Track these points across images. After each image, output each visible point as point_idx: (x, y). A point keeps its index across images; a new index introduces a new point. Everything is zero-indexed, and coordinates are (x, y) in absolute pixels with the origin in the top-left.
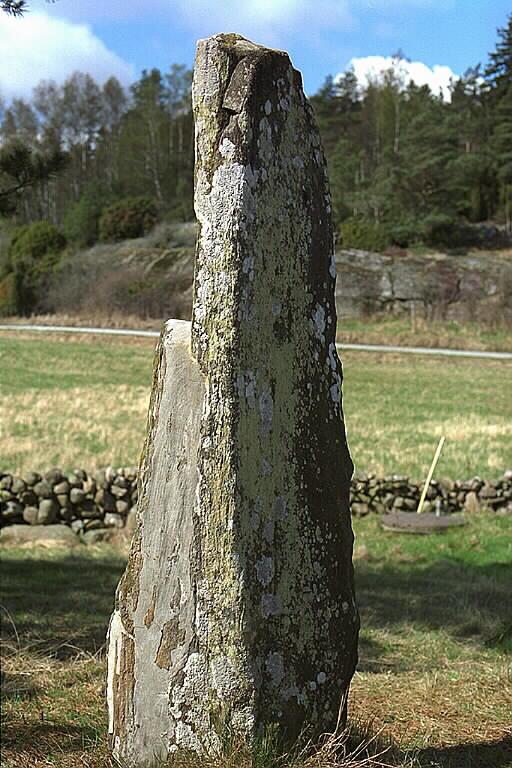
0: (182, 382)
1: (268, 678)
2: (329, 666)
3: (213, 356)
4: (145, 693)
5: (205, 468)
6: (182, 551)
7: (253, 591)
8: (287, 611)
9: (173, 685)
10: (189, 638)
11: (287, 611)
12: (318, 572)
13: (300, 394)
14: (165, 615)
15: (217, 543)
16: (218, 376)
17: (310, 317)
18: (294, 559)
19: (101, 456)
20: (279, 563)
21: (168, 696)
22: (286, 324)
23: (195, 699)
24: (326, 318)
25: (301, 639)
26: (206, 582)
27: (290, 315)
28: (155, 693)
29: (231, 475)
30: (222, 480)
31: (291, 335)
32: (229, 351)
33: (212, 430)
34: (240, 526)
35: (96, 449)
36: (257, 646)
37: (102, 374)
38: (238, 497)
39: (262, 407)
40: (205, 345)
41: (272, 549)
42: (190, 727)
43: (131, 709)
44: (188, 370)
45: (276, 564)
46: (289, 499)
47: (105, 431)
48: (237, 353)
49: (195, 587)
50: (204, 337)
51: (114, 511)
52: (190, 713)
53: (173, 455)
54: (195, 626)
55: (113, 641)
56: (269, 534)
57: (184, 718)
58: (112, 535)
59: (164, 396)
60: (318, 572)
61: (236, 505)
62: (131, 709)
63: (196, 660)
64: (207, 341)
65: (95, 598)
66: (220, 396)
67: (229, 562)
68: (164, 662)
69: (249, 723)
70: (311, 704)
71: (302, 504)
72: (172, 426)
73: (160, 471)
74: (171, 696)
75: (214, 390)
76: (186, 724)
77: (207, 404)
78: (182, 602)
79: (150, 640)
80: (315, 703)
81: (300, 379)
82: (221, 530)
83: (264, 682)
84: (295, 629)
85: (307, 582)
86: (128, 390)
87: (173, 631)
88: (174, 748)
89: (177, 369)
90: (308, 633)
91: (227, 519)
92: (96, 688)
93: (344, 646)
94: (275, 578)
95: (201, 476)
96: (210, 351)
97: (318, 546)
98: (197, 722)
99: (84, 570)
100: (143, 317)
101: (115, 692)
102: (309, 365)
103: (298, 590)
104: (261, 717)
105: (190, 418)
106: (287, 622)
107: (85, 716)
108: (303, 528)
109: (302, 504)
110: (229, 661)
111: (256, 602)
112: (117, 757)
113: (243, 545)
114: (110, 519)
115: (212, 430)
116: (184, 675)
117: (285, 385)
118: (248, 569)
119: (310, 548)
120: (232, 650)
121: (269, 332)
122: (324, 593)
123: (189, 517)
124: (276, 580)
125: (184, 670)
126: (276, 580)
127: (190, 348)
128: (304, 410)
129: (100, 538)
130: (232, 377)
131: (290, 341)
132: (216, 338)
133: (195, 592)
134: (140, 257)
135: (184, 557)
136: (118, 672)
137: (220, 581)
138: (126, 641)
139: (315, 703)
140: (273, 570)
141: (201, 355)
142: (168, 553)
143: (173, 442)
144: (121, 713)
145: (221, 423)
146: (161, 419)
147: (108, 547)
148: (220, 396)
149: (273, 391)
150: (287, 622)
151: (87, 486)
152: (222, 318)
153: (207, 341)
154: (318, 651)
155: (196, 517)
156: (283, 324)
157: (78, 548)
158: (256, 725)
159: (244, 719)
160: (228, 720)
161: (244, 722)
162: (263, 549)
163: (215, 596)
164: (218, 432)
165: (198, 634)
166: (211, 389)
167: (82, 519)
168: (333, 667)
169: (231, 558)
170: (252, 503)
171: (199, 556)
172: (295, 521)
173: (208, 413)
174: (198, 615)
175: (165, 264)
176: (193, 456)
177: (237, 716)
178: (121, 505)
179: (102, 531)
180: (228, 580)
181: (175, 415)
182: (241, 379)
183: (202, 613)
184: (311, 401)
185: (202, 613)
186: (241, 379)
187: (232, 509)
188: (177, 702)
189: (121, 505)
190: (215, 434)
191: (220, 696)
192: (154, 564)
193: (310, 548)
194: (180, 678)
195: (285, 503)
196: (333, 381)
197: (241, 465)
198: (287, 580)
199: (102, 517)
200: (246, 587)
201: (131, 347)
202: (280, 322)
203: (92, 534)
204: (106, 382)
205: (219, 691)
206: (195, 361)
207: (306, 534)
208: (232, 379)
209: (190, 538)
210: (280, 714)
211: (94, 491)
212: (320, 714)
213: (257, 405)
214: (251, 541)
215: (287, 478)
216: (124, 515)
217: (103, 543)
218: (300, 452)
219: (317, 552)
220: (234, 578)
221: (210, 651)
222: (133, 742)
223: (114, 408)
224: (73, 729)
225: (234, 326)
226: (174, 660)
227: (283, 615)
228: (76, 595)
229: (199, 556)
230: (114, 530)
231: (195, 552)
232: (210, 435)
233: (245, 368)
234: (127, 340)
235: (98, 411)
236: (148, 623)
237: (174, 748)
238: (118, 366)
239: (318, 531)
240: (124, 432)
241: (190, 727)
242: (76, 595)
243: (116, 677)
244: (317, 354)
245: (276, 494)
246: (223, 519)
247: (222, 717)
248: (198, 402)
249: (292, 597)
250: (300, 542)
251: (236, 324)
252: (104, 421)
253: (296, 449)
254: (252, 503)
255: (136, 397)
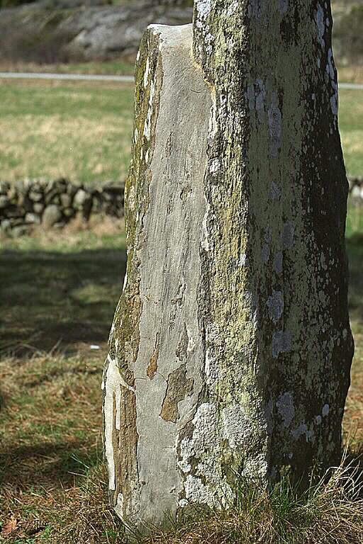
0: (183, 94)
1: (280, 421)
2: (332, 398)
3: (219, 59)
4: (151, 448)
5: (213, 195)
6: (188, 292)
7: (266, 330)
8: (296, 347)
9: (181, 438)
10: (198, 388)
11: (296, 347)
12: (323, 301)
13: (305, 106)
14: (170, 364)
15: (227, 280)
16: (226, 85)
17: (312, 18)
18: (302, 291)
19: (17, 169)
20: (288, 296)
21: (175, 449)
22: (293, 24)
23: (206, 451)
24: (325, 20)
25: (309, 374)
26: (216, 325)
27: (297, 14)
28: (161, 445)
29: (242, 203)
30: (232, 207)
31: (298, 37)
32: (238, 54)
33: (220, 150)
34: (253, 260)
35: (13, 164)
36: (269, 389)
37: (13, 107)
38: (251, 227)
39: (271, 121)
40: (210, 48)
41: (281, 282)
42: (199, 480)
43: (135, 466)
44: (191, 79)
45: (285, 297)
46: (296, 226)
47: (18, 151)
48: (248, 58)
49: (204, 331)
50: (209, 38)
51: (32, 211)
52: (200, 467)
53: (174, 182)
54: (204, 374)
55: (109, 393)
56: (278, 267)
57: (193, 472)
58: (32, 230)
59: (162, 111)
60: (323, 301)
61: (248, 237)
62: (135, 466)
63: (205, 411)
64: (212, 43)
65: (33, 289)
66: (229, 109)
67: (242, 302)
68: (170, 412)
69: (262, 470)
70: (317, 439)
71: (309, 229)
72: (172, 147)
73: (160, 199)
74: (179, 450)
75: (222, 102)
76: (197, 477)
77: (214, 118)
78: (189, 349)
79: (153, 391)
80: (321, 437)
81: (306, 87)
82: (232, 265)
83: (276, 425)
84: (303, 365)
85: (314, 313)
86: (33, 119)
87: (180, 382)
88: (183, 503)
89: (177, 78)
90: (315, 366)
91: (239, 253)
92: (58, 390)
93: (344, 374)
94: (284, 313)
95: (209, 205)
96: (217, 54)
97: (322, 273)
98: (208, 474)
99: (19, 263)
100: (40, 63)
101: (116, 448)
102: (314, 74)
103: (306, 323)
104: (272, 461)
105: (194, 137)
106: (296, 358)
107: (61, 426)
108: (310, 256)
109: (309, 229)
110: (242, 409)
111: (267, 342)
112: (121, 515)
113: (255, 281)
114: (30, 217)
115: (220, 150)
116: (193, 427)
117: (292, 96)
118: (261, 307)
119: (316, 277)
120: (244, 397)
121: (276, 33)
122: (328, 323)
123: (195, 252)
124: (285, 316)
125: (194, 422)
126: (285, 316)
127: (191, 53)
128: (309, 124)
129: (23, 233)
130: (242, 87)
131: (296, 44)
132: (223, 38)
133: (204, 338)
134: (35, 18)
135: (191, 298)
136: (118, 427)
137: (231, 324)
138: (126, 393)
139: (321, 437)
140: (283, 305)
141: (206, 58)
142: (171, 296)
143: (174, 166)
144: (123, 469)
145: (230, 141)
146: (158, 140)
147: (30, 240)
148: (229, 109)
149: (281, 102)
150: (296, 358)
151: (11, 193)
152: (229, 14)
153: (212, 43)
154: (323, 384)
155: (203, 253)
156: (290, 23)
157: (9, 241)
158: (269, 470)
159: (257, 467)
160: (241, 469)
161: (257, 470)
162: (273, 283)
163: (226, 340)
164: (228, 152)
165: (208, 383)
166: (218, 100)
167: (8, 218)
168: (335, 397)
169: (244, 297)
170: (263, 233)
171: (207, 297)
172: (302, 249)
173: (216, 130)
174: (208, 362)
175: (54, 22)
176: (198, 183)
177: (249, 465)
178: (38, 207)
179: (24, 227)
180: (241, 322)
181: (175, 134)
182: (251, 89)
183: (212, 359)
184: (316, 114)
185: (212, 359)
186: (251, 89)
187: (244, 242)
188: (185, 455)
189: (38, 207)
190: (225, 156)
191: (232, 446)
192: (156, 309)
193: (316, 277)
194: (188, 431)
195: (293, 229)
196: (332, 91)
197: (253, 191)
198: (295, 315)
199: (24, 217)
200: (259, 328)
201: (32, 86)
202: (287, 21)
203: (17, 230)
204: (16, 114)
205: (232, 441)
206: (199, 67)
207: (312, 262)
208: (243, 87)
209: (196, 276)
210: (291, 456)
211: (16, 197)
212: (325, 446)
213: (267, 119)
214: (263, 276)
215: (295, 202)
216: (40, 215)
217: (26, 237)
218: (307, 173)
219: (322, 280)
220: (247, 319)
221: (221, 401)
222: (138, 499)
223: (24, 132)
224: (48, 450)
225: (243, 24)
226: (182, 412)
227: (292, 352)
228: (17, 289)
229: (207, 297)
230: (33, 226)
231: (203, 292)
232: (218, 156)
233: (254, 74)
234: (29, 81)
235: (11, 136)
236: (152, 371)
237: (183, 503)
238: (23, 101)
239: (323, 258)
240: (33, 150)
241: (199, 480)
242: (17, 289)
243: (116, 432)
244: (319, 61)
245: (284, 219)
246: (235, 254)
247: (234, 468)
248: (204, 116)
249: (301, 332)
250: (308, 270)
251: (246, 21)
252: (17, 143)
253: (303, 168)
254: (263, 233)
255: (39, 124)
